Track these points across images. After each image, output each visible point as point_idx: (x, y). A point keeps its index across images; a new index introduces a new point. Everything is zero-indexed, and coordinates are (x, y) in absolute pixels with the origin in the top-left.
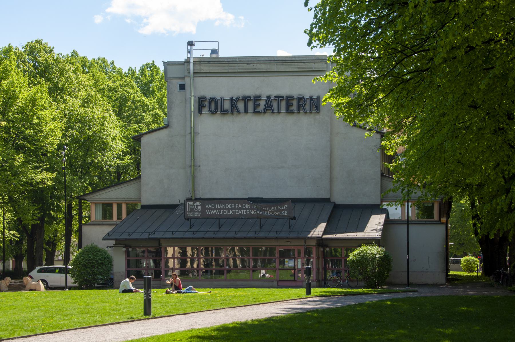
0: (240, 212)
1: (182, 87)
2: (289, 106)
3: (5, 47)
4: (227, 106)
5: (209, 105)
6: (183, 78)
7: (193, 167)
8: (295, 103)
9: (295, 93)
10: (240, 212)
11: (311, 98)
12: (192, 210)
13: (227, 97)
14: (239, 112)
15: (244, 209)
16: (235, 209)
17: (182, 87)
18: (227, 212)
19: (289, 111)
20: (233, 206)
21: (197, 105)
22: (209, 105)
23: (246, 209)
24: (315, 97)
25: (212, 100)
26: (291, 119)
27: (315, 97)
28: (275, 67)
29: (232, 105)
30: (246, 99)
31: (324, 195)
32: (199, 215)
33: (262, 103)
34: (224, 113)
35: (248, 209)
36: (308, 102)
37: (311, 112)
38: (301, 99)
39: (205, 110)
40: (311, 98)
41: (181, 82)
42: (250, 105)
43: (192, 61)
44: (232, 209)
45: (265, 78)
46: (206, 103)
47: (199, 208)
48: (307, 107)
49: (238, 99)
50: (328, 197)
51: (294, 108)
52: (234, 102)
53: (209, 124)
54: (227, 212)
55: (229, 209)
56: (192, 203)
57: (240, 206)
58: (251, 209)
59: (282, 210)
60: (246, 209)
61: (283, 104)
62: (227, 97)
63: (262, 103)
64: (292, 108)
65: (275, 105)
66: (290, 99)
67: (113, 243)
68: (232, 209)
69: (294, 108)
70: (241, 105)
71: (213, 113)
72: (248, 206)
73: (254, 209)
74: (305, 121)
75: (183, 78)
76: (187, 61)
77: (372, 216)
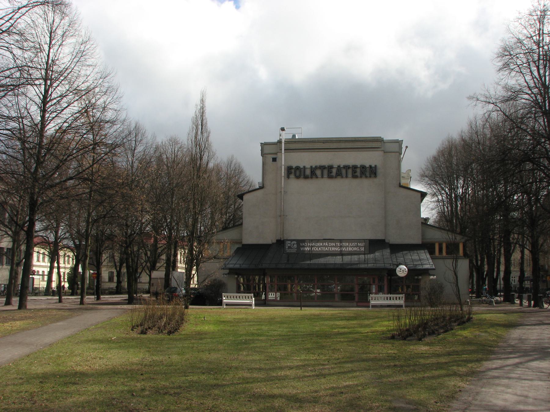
0: (327, 249)
1: (274, 160)
2: (354, 172)
3: (154, 137)
4: (308, 172)
5: (294, 172)
6: (276, 154)
7: (282, 217)
8: (358, 170)
9: (359, 163)
10: (327, 249)
11: (371, 167)
12: (290, 247)
13: (308, 166)
14: (317, 177)
15: (330, 247)
16: (323, 246)
17: (274, 160)
18: (317, 249)
19: (354, 177)
20: (321, 244)
21: (286, 172)
22: (294, 172)
23: (331, 246)
24: (373, 166)
25: (298, 168)
26: (355, 182)
27: (373, 166)
28: (343, 145)
29: (312, 172)
30: (322, 168)
31: (380, 237)
32: (294, 251)
33: (334, 171)
34: (306, 177)
35: (333, 246)
36: (368, 170)
37: (370, 177)
38: (363, 167)
39: (292, 176)
40: (371, 167)
41: (274, 156)
42: (326, 172)
43: (283, 141)
44: (321, 246)
45: (336, 153)
46: (293, 171)
47: (295, 246)
48: (368, 174)
49: (316, 168)
50: (383, 238)
51: (358, 173)
52: (313, 170)
53: (295, 184)
54: (317, 249)
55: (318, 247)
56: (290, 242)
57: (327, 244)
58: (336, 246)
59: (361, 246)
60: (331, 246)
61: (350, 171)
62: (308, 166)
63: (334, 171)
64: (356, 174)
65: (344, 171)
66: (355, 167)
67: (227, 271)
68: (321, 246)
69: (358, 173)
70: (318, 172)
71: (298, 177)
72: (333, 244)
73: (338, 247)
74: (366, 182)
75: (276, 154)
76: (280, 142)
77: (426, 251)
